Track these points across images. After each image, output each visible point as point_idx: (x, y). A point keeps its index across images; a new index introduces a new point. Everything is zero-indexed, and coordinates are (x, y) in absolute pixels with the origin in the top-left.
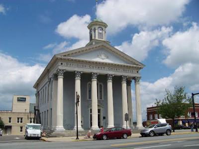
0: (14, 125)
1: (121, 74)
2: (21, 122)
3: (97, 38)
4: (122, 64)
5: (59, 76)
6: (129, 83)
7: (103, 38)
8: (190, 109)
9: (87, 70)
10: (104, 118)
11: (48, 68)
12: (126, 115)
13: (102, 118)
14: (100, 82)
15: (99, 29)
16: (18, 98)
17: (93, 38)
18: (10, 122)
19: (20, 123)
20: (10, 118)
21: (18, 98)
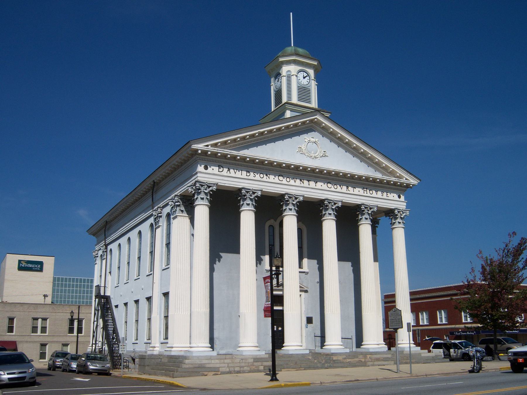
0: (27, 339)
1: (323, 197)
2: (44, 329)
3: (295, 100)
4: (378, 175)
5: (197, 203)
6: (374, 224)
7: (309, 102)
8: (508, 299)
9: (273, 184)
10: (309, 320)
11: (156, 178)
12: (98, 287)
13: (317, 321)
14: (300, 223)
15: (301, 75)
16: (20, 261)
17: (284, 100)
18: (10, 329)
19: (39, 333)
20: (11, 320)
21: (20, 261)
